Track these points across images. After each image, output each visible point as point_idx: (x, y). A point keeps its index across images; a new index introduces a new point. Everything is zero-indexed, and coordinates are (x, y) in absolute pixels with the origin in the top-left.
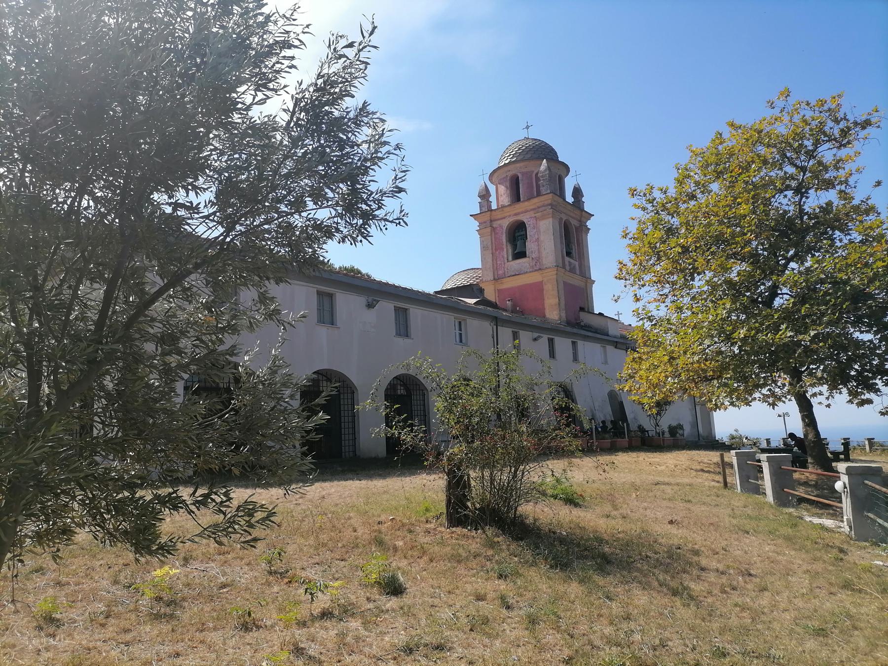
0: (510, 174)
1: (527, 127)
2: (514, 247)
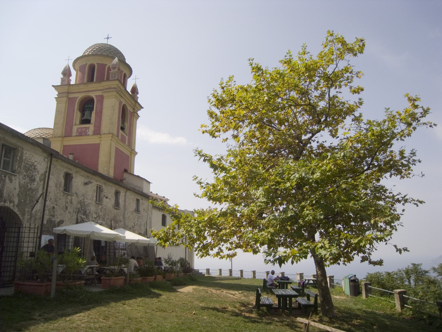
0: (89, 63)
1: (108, 38)
2: (83, 115)
